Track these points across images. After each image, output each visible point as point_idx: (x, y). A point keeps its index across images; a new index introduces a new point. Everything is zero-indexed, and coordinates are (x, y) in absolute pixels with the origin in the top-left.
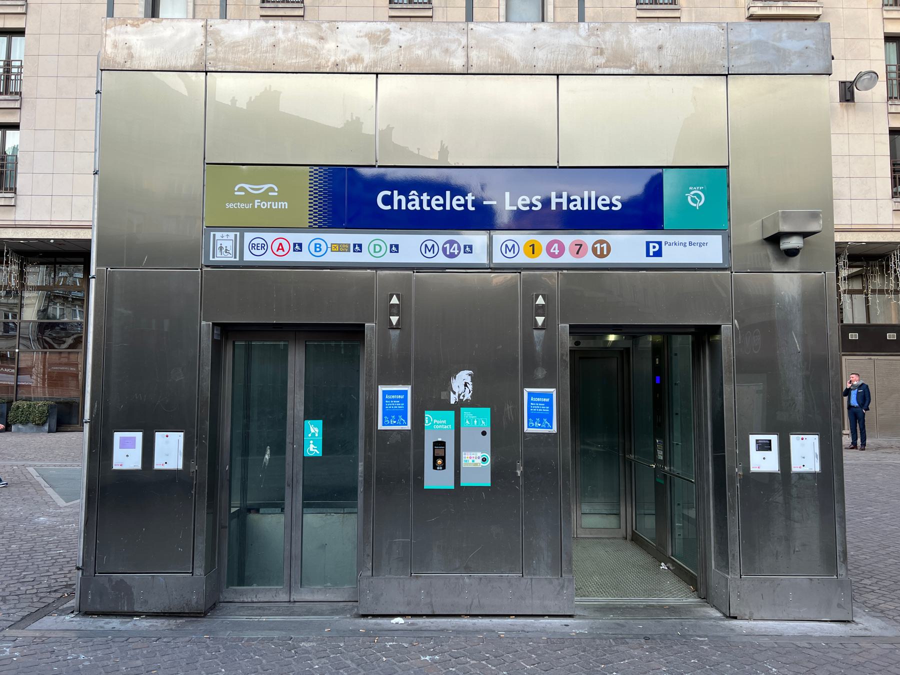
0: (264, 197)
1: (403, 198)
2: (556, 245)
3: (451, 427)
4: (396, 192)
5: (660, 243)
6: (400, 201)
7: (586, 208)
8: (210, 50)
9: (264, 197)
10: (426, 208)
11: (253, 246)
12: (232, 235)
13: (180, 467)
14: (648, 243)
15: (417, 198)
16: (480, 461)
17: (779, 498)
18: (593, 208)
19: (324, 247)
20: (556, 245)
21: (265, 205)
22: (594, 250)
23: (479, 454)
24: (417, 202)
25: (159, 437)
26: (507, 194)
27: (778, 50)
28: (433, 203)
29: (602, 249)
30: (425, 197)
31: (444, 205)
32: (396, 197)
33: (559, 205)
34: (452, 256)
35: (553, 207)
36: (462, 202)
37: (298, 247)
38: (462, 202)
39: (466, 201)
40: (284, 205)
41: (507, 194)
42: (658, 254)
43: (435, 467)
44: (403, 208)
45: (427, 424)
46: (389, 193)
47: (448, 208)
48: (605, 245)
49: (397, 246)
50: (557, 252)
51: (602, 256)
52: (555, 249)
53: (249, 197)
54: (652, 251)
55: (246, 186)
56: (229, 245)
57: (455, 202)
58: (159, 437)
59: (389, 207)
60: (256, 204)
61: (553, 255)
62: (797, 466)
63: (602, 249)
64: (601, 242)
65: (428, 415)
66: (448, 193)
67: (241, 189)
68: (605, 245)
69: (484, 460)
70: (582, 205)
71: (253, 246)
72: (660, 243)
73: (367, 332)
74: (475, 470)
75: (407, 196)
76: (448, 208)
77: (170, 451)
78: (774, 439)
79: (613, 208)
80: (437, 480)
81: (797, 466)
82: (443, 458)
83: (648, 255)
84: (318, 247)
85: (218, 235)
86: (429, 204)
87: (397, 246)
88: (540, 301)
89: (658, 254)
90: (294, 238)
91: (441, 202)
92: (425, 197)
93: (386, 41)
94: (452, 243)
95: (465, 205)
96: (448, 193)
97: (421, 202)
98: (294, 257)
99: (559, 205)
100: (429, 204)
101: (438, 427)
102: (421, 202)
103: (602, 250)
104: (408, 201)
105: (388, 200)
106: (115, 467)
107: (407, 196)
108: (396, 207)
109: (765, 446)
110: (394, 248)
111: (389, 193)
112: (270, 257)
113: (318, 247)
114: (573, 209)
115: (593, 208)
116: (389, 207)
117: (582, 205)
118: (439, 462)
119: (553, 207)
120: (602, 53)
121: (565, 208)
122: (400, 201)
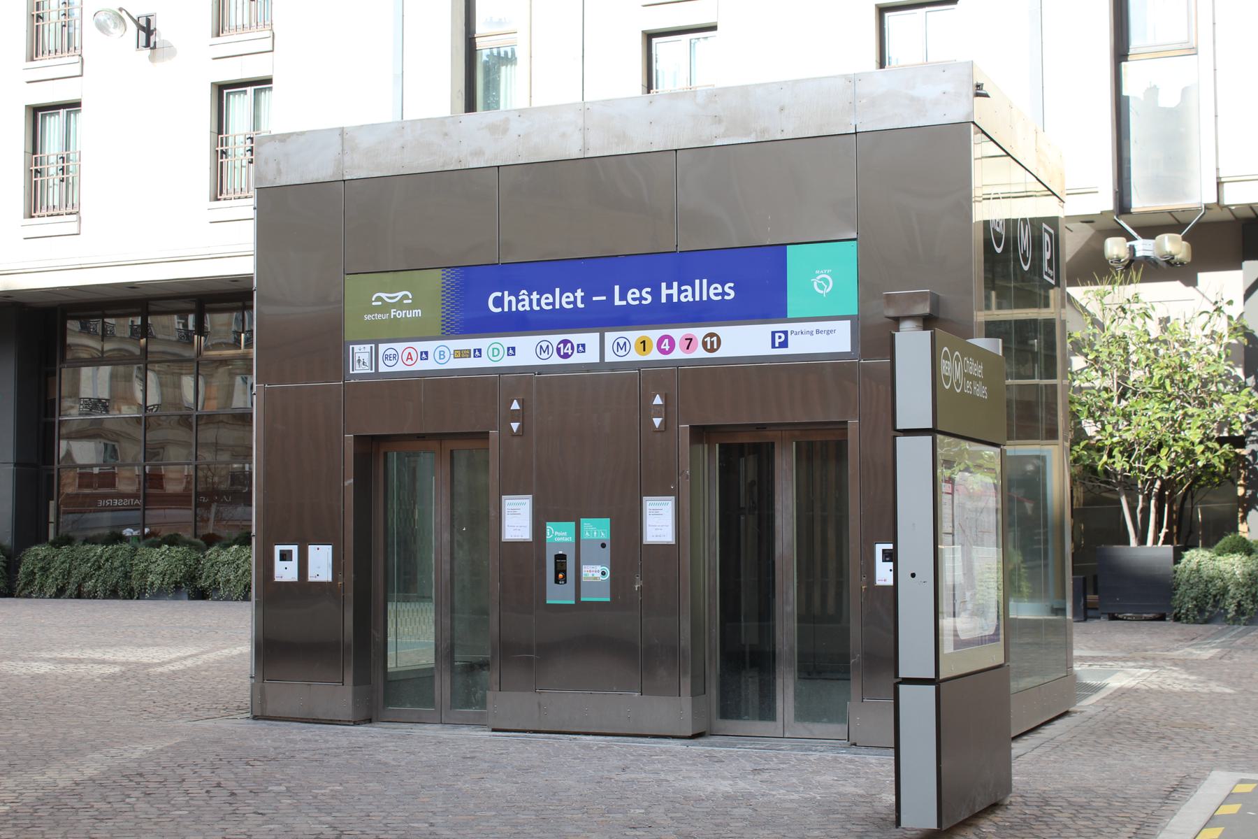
0: (400, 305)
1: (513, 299)
2: (666, 341)
3: (571, 539)
4: (506, 293)
5: (786, 333)
6: (510, 302)
7: (697, 299)
8: (346, 158)
9: (400, 305)
10: (536, 308)
11: (387, 357)
12: (368, 347)
13: (330, 579)
14: (773, 333)
15: (527, 298)
16: (599, 575)
18: (705, 298)
19: (447, 354)
20: (666, 341)
21: (400, 314)
23: (599, 568)
24: (527, 303)
25: (312, 549)
26: (617, 288)
27: (912, 99)
28: (543, 301)
29: (712, 343)
30: (535, 296)
31: (553, 304)
32: (507, 299)
33: (669, 297)
34: (566, 356)
36: (572, 299)
38: (572, 299)
39: (575, 298)
41: (617, 288)
42: (784, 344)
43: (557, 581)
44: (514, 309)
45: (548, 537)
46: (499, 294)
47: (557, 306)
48: (715, 339)
49: (513, 349)
50: (667, 348)
51: (712, 350)
53: (386, 307)
54: (777, 341)
55: (383, 295)
56: (365, 357)
58: (312, 549)
59: (499, 310)
61: (663, 352)
62: (312, 576)
63: (712, 343)
64: (711, 335)
65: (550, 527)
67: (377, 300)
68: (715, 339)
69: (603, 573)
70: (694, 296)
71: (387, 357)
73: (491, 438)
74: (594, 584)
75: (517, 296)
76: (557, 306)
78: (294, 549)
79: (726, 298)
80: (559, 595)
81: (312, 576)
82: (565, 572)
83: (773, 346)
84: (442, 354)
85: (357, 347)
86: (539, 304)
87: (513, 349)
88: (515, 406)
90: (421, 346)
91: (551, 300)
92: (535, 296)
93: (505, 131)
94: (565, 342)
95: (575, 303)
97: (531, 301)
98: (421, 366)
99: (669, 297)
100: (539, 304)
101: (560, 539)
102: (531, 301)
104: (518, 301)
105: (499, 302)
106: (310, 579)
107: (517, 296)
108: (506, 309)
109: (285, 556)
111: (499, 294)
112: (400, 367)
113: (442, 354)
114: (521, 309)
115: (705, 298)
116: (499, 310)
117: (694, 296)
118: (561, 576)
119: (664, 300)
121: (675, 300)
122: (510, 302)
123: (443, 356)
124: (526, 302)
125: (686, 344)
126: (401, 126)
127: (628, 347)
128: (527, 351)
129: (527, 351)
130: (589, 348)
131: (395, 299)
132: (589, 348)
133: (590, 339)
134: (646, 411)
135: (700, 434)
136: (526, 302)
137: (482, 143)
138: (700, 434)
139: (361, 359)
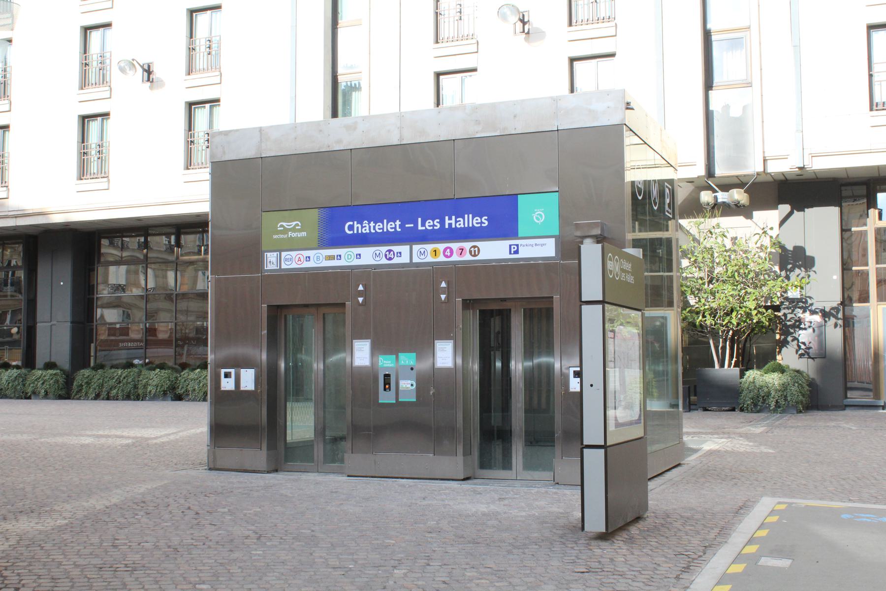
0: (294, 230)
1: (359, 226)
5: (517, 245)
9: (294, 230)
10: (373, 231)
11: (286, 260)
12: (275, 254)
14: (510, 246)
16: (409, 386)
17: (150, 441)
19: (302, 259)
21: (294, 235)
22: (470, 252)
23: (410, 382)
24: (367, 228)
26: (420, 220)
28: (377, 227)
30: (372, 224)
31: (383, 229)
32: (356, 226)
33: (450, 225)
34: (390, 259)
35: (447, 226)
37: (308, 258)
40: (304, 234)
41: (420, 220)
42: (516, 252)
43: (385, 389)
46: (351, 223)
51: (475, 255)
52: (448, 253)
53: (286, 231)
54: (513, 250)
55: (284, 224)
56: (274, 260)
57: (475, 221)
60: (447, 222)
61: (447, 256)
66: (385, 221)
71: (286, 260)
72: (517, 245)
74: (407, 391)
77: (248, 379)
80: (386, 398)
82: (389, 384)
83: (510, 253)
84: (318, 258)
85: (269, 254)
89: (516, 252)
92: (372, 224)
93: (355, 128)
95: (395, 228)
96: (385, 221)
99: (450, 225)
103: (475, 252)
104: (362, 227)
105: (351, 228)
110: (359, 256)
111: (351, 223)
112: (294, 266)
113: (318, 258)
114: (458, 226)
119: (447, 226)
120: (479, 124)
121: (453, 226)
123: (319, 259)
124: (367, 228)
125: (460, 252)
126: (295, 126)
127: (425, 254)
128: (368, 256)
129: (368, 256)
130: (403, 254)
131: (291, 226)
132: (403, 254)
133: (404, 249)
134: (437, 291)
135: (468, 304)
136: (367, 228)
137: (340, 136)
138: (468, 304)
139: (271, 261)
